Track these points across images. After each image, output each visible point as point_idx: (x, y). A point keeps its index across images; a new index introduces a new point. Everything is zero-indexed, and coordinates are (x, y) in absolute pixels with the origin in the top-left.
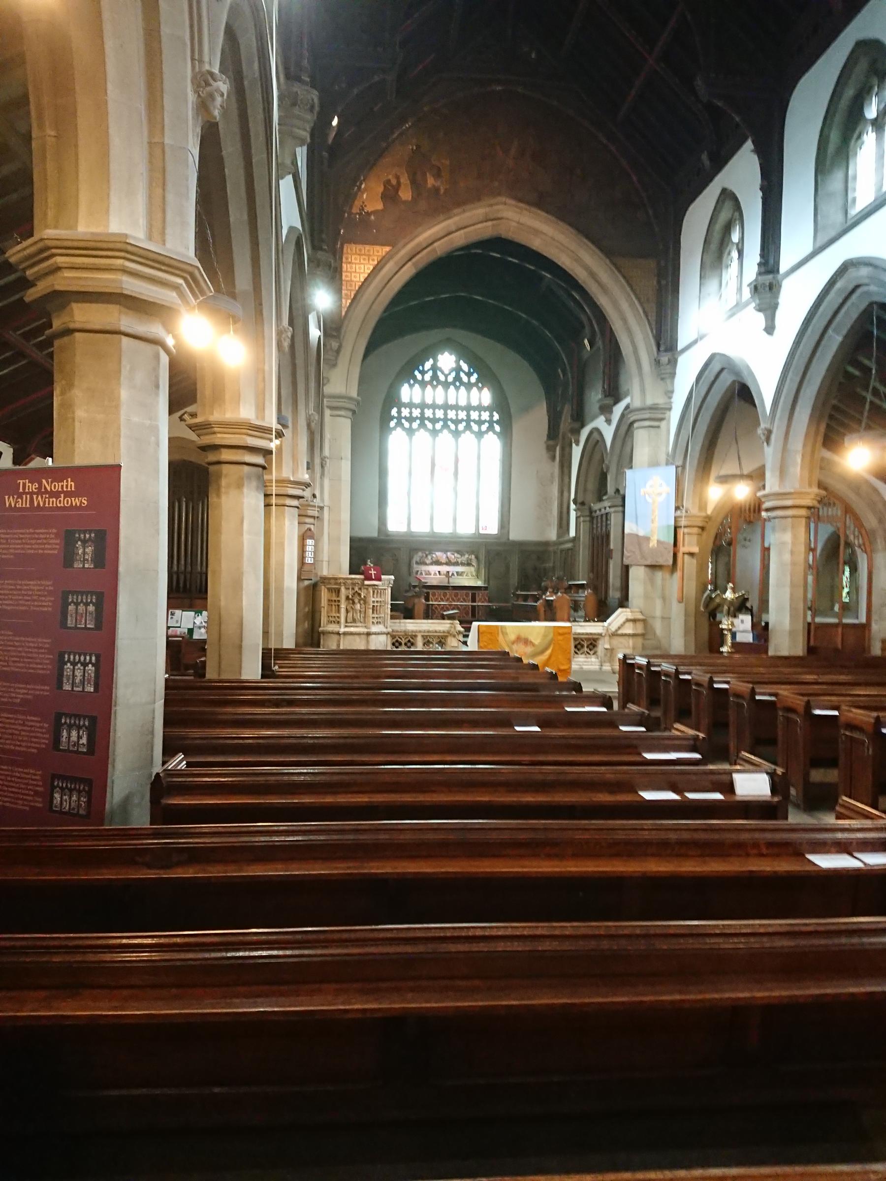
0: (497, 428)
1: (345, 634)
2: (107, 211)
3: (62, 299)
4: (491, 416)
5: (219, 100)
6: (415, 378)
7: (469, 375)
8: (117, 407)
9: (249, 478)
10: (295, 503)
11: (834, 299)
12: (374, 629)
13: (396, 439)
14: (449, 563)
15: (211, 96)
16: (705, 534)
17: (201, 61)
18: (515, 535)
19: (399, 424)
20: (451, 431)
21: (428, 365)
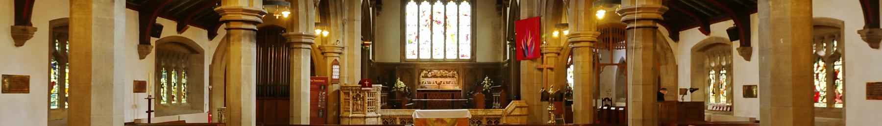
1: (352, 117)
9: (245, 35)
14: (442, 77)
16: (560, 58)
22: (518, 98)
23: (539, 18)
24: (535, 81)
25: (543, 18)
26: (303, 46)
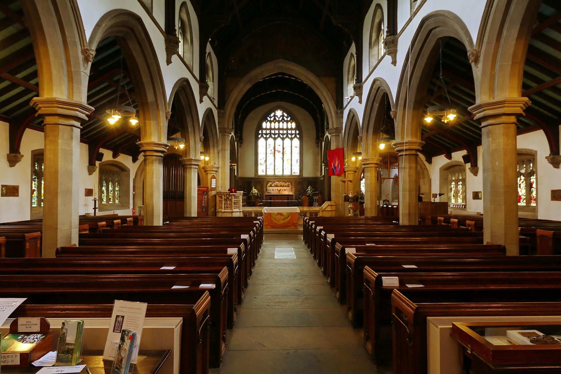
0: (298, 136)
1: (224, 212)
2: (52, 91)
3: (42, 116)
4: (296, 132)
5: (91, 56)
6: (267, 119)
7: (287, 117)
8: (58, 145)
9: (156, 160)
10: (197, 167)
11: (374, 92)
12: (234, 210)
13: (261, 142)
14: (281, 186)
15: (89, 56)
16: (356, 174)
17: (84, 46)
18: (305, 175)
19: (262, 136)
20: (281, 138)
21: (272, 115)
22: (330, 200)
23: (343, 149)
24: (340, 189)
25: (345, 149)
26: (193, 166)
